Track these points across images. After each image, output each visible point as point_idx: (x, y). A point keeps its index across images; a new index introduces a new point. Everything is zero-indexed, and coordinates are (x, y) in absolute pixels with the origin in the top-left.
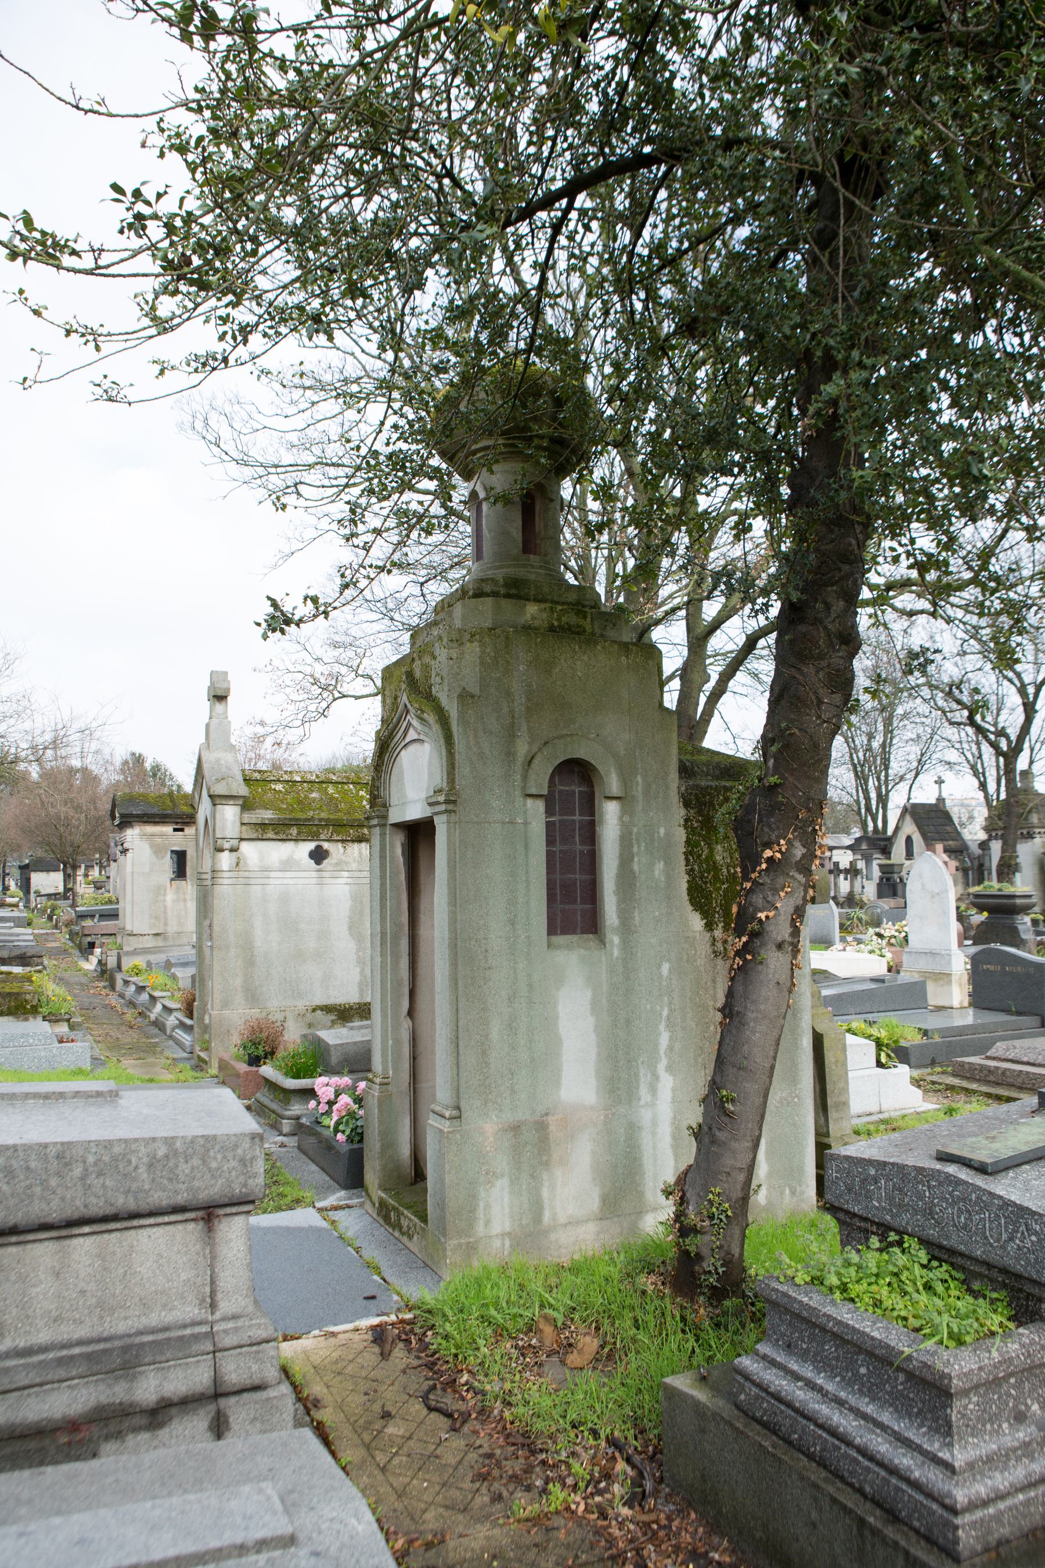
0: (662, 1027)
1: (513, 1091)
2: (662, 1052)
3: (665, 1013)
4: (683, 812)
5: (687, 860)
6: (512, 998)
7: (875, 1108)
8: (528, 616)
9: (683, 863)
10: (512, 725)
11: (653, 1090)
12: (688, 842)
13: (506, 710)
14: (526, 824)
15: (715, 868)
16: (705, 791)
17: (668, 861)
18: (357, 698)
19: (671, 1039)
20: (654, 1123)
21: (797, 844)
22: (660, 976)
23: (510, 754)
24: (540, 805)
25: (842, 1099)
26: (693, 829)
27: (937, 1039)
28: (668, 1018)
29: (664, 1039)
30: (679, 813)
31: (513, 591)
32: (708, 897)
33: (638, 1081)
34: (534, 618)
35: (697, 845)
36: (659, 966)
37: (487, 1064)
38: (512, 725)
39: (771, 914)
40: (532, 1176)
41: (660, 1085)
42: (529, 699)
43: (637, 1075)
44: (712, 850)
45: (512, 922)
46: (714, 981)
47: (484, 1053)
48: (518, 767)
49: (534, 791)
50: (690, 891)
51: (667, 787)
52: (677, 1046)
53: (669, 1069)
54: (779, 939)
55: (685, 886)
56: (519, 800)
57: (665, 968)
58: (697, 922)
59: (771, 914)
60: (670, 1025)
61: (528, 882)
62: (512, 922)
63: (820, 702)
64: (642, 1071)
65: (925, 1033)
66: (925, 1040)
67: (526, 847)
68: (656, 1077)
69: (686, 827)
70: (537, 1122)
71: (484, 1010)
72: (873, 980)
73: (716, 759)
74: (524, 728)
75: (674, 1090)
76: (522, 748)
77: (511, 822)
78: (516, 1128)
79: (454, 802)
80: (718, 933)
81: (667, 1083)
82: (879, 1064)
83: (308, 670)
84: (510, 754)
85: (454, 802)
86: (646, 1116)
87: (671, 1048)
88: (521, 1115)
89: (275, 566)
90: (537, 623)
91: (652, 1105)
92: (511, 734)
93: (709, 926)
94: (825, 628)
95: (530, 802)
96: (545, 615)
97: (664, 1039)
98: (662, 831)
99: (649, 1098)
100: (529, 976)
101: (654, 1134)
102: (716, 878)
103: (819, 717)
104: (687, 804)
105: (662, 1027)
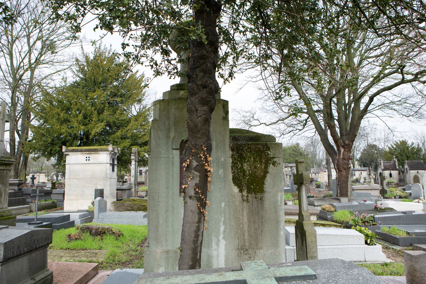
0: (221, 224)
1: (166, 240)
2: (221, 232)
3: (223, 219)
4: (231, 153)
5: (232, 169)
6: (167, 211)
7: (363, 260)
8: (181, 95)
9: (231, 169)
10: (169, 128)
11: (218, 245)
12: (233, 162)
13: (167, 123)
14: (173, 158)
15: (244, 172)
16: (240, 145)
17: (225, 169)
18: (255, 126)
19: (225, 228)
20: (218, 256)
21: (194, 161)
22: (221, 207)
23: (168, 137)
24: (178, 152)
25: (314, 255)
26: (235, 159)
27: (414, 236)
28: (224, 221)
29: (222, 228)
30: (229, 153)
31: (180, 88)
32: (240, 181)
33: (212, 241)
34: (182, 95)
35: (237, 163)
36: (221, 204)
37: (158, 231)
38: (169, 128)
39: (186, 186)
40: (172, 268)
41: (220, 243)
42: (175, 120)
43: (211, 239)
44: (242, 165)
45: (167, 188)
46: (243, 210)
47: (157, 227)
48: (171, 141)
49: (174, 148)
50: (234, 179)
51: (225, 145)
52: (227, 230)
53: (224, 238)
54: (190, 195)
55: (231, 177)
56: (171, 151)
57: (223, 204)
58: (236, 189)
59: (186, 186)
60: (225, 223)
61: (173, 176)
62: (167, 188)
63: (197, 110)
64: (213, 238)
65: (408, 233)
66: (408, 236)
67: (173, 165)
68: (219, 241)
69: (232, 157)
70: (174, 251)
71: (158, 214)
72: (403, 213)
73: (255, 135)
74: (173, 128)
75: (226, 245)
76: (172, 135)
77: (168, 157)
78: (167, 252)
79: (150, 152)
80: (245, 193)
81: (223, 243)
82: (366, 243)
83: (243, 120)
84: (168, 137)
85: (150, 152)
86: (215, 253)
87: (225, 231)
88: (169, 248)
89: (237, 92)
90: (183, 97)
91: (217, 250)
92: (169, 131)
93: (241, 191)
94: (196, 83)
95: (174, 151)
96: (186, 94)
97: (222, 228)
98: (223, 159)
99: (216, 247)
100: (173, 205)
101: (218, 259)
102: (244, 175)
103: (197, 115)
104: (232, 150)
105: (221, 224)
